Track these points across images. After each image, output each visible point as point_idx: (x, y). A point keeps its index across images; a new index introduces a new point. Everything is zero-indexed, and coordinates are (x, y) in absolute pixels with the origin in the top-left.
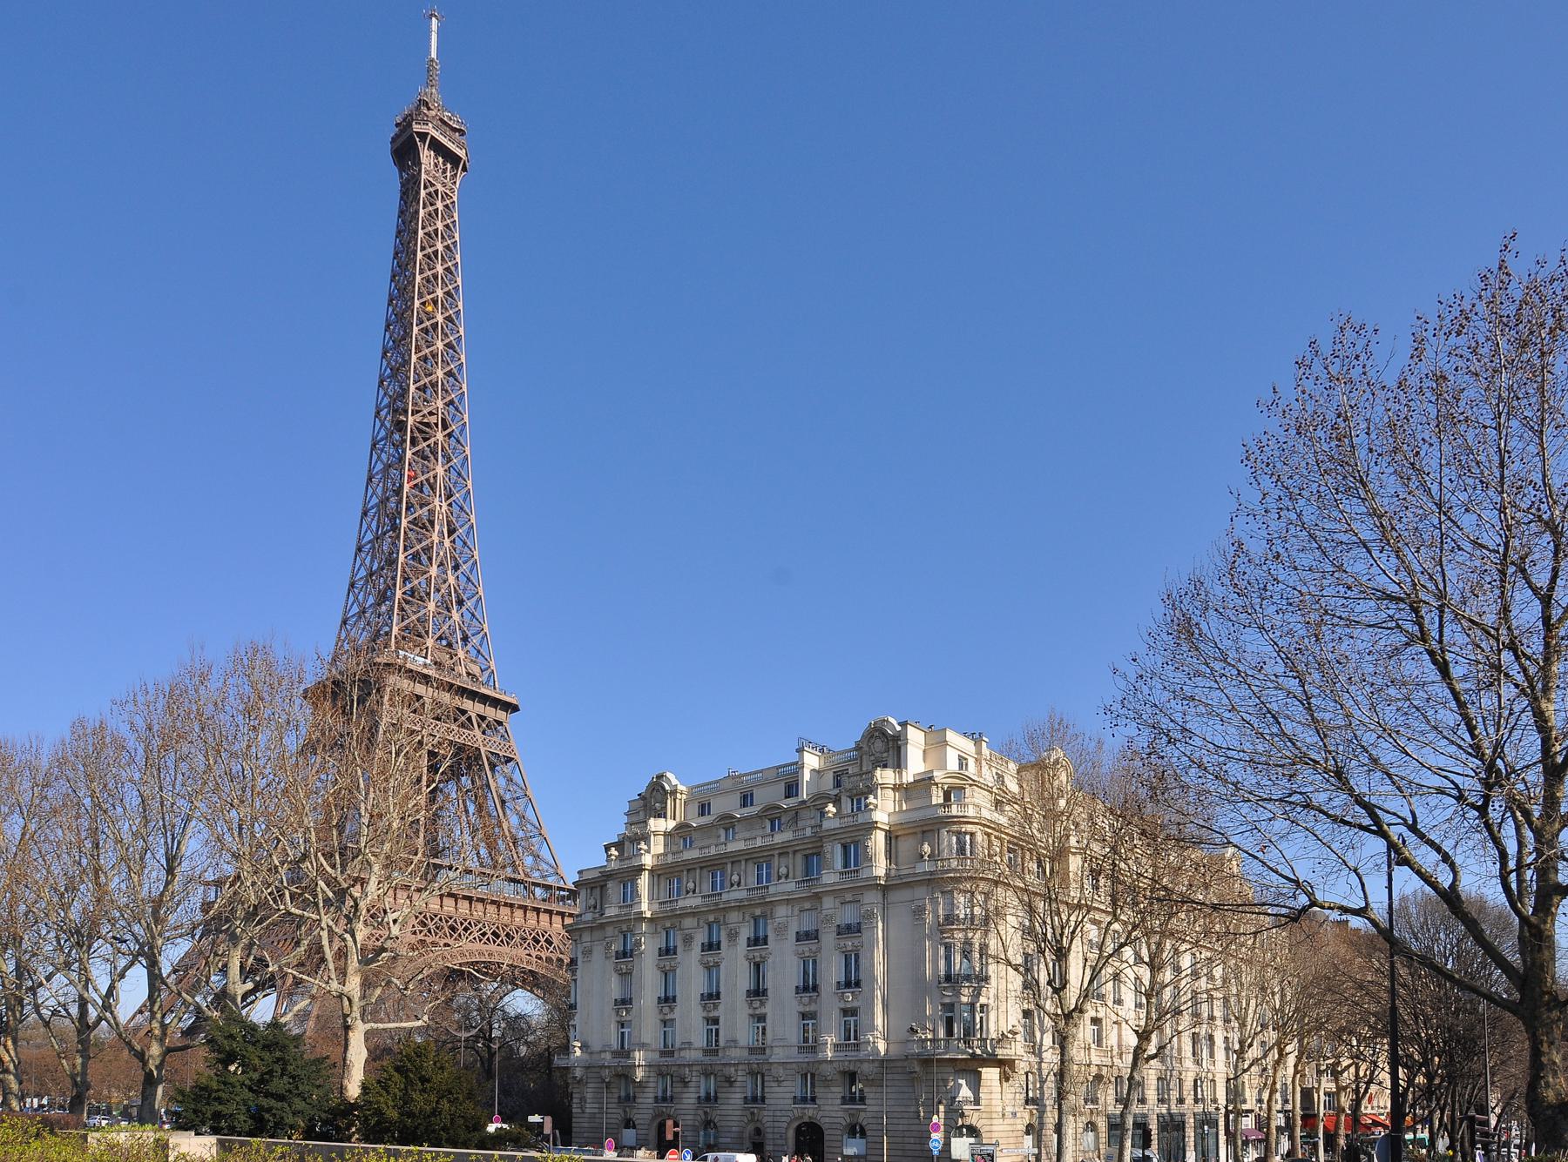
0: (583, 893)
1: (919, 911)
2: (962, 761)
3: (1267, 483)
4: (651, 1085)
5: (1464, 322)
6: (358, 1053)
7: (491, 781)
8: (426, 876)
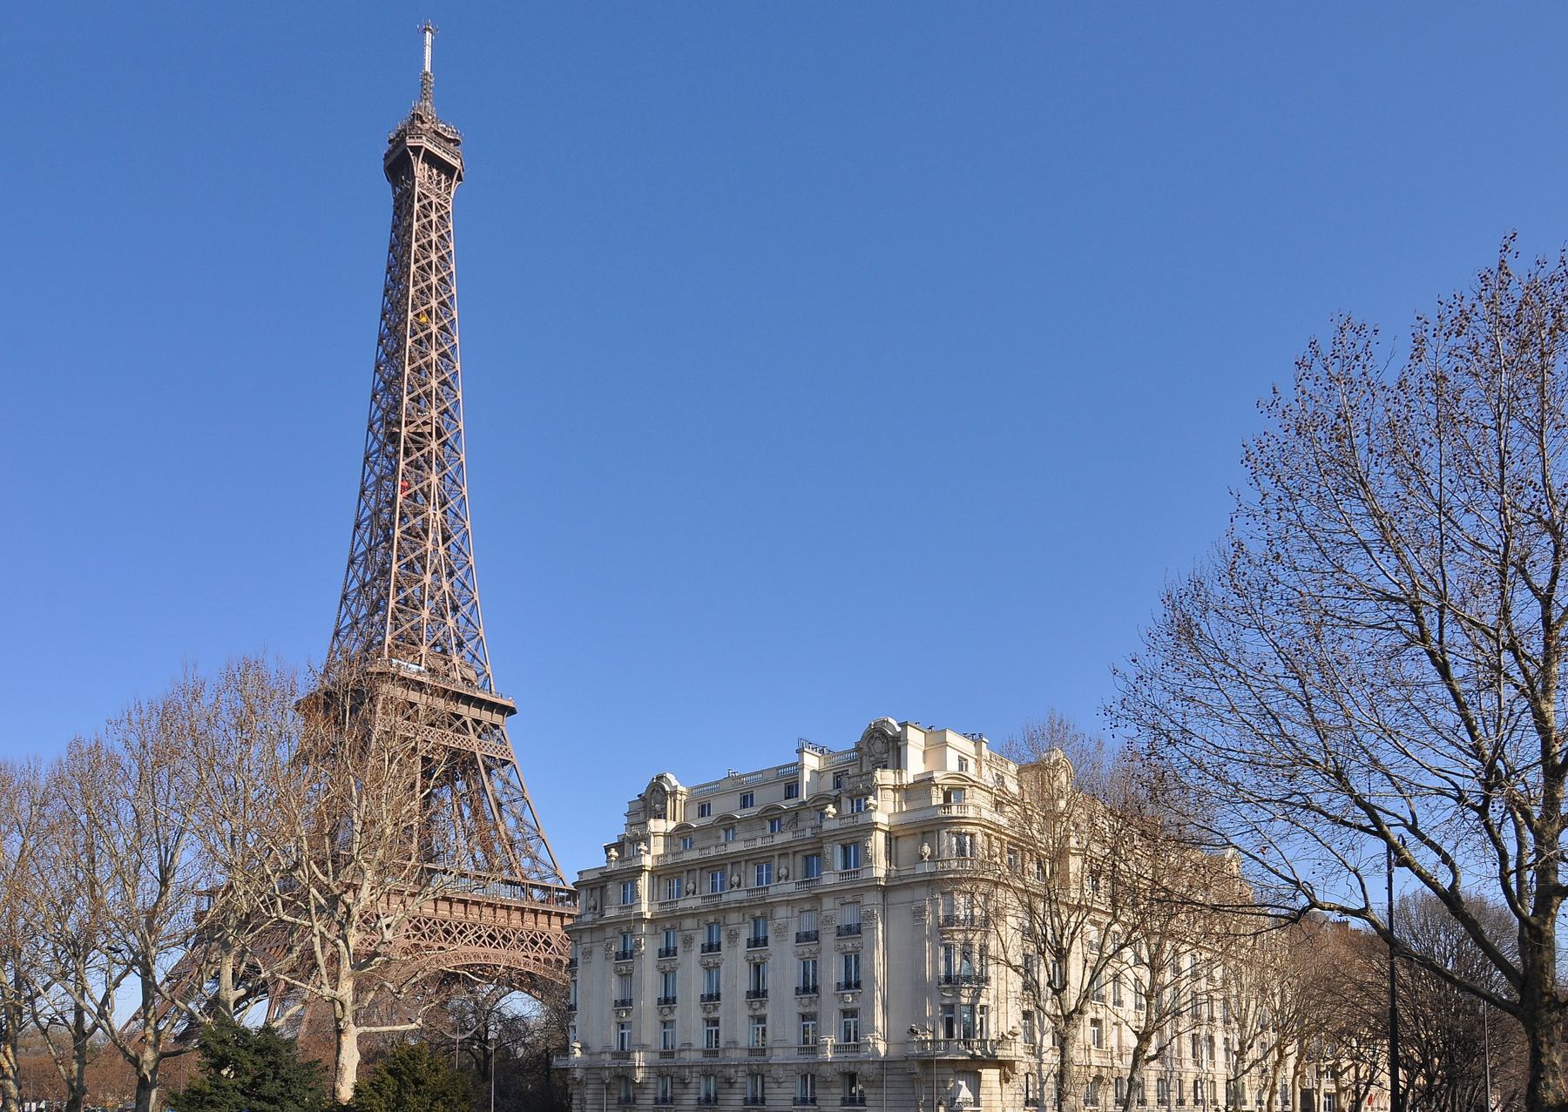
0: (583, 894)
1: (919, 913)
2: (962, 762)
3: (1267, 483)
4: (652, 1086)
5: (1464, 322)
6: (350, 1057)
8: (420, 880)
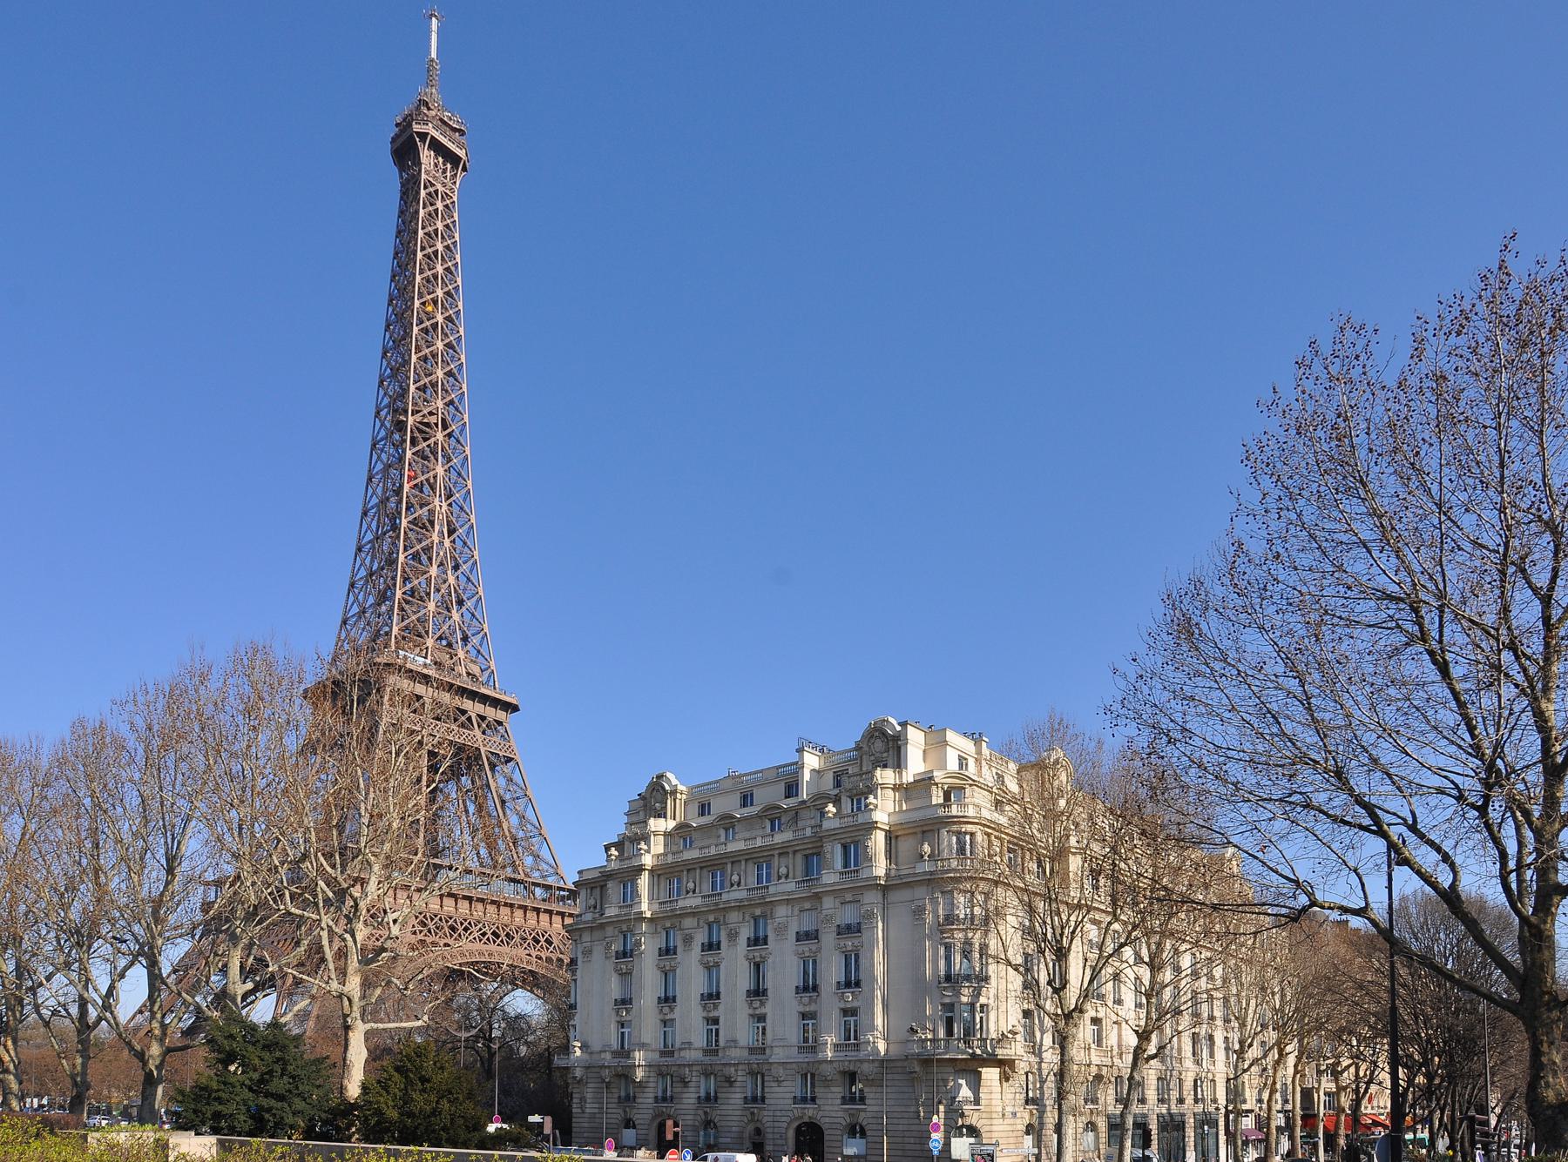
0: (583, 893)
1: (919, 911)
2: (962, 761)
3: (1267, 483)
4: (651, 1085)
5: (1464, 322)
6: (358, 1053)
7: (491, 781)
8: (426, 876)
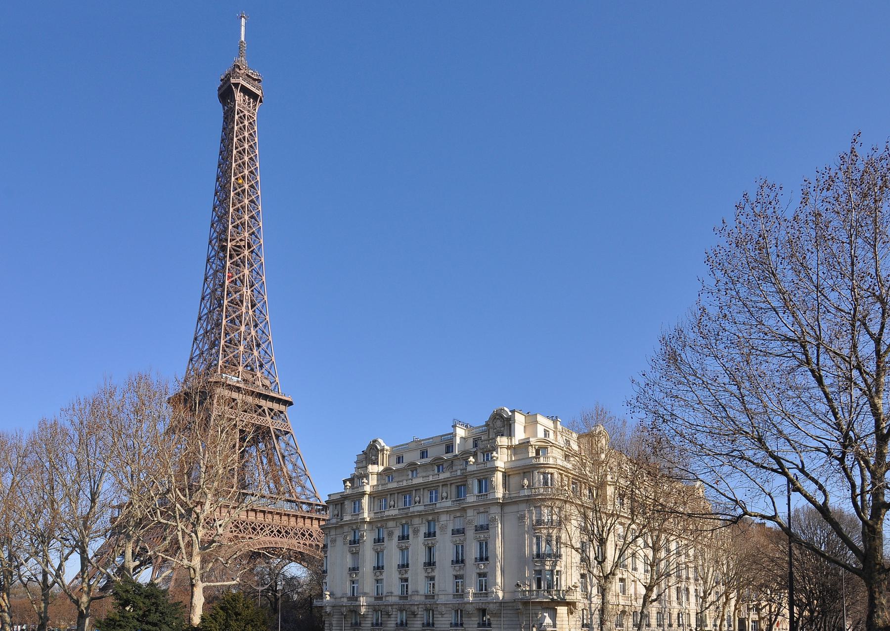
0: (331, 507)
1: (522, 518)
2: (546, 432)
3: (719, 274)
4: (370, 616)
5: (831, 183)
6: (199, 600)
8: (238, 500)
